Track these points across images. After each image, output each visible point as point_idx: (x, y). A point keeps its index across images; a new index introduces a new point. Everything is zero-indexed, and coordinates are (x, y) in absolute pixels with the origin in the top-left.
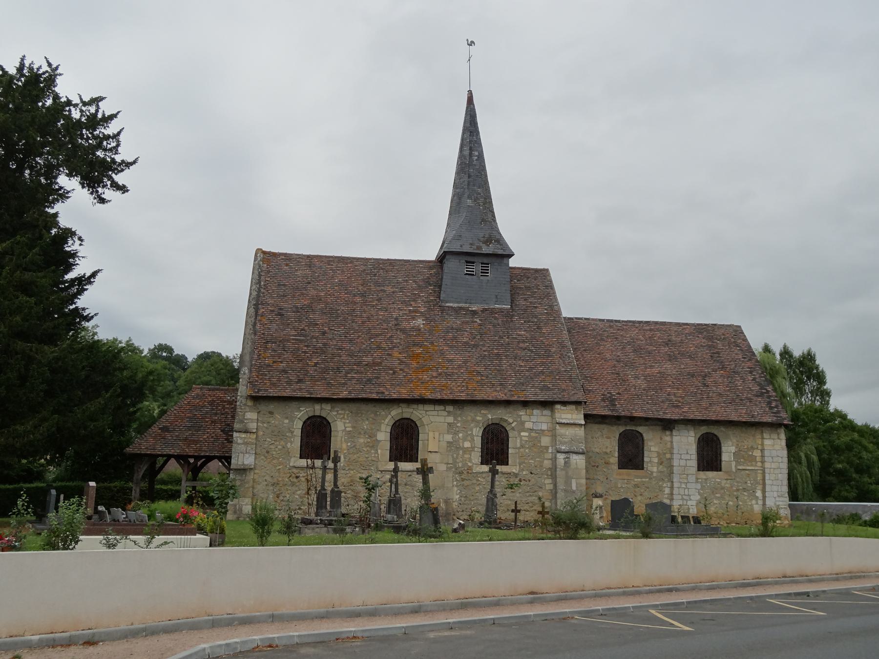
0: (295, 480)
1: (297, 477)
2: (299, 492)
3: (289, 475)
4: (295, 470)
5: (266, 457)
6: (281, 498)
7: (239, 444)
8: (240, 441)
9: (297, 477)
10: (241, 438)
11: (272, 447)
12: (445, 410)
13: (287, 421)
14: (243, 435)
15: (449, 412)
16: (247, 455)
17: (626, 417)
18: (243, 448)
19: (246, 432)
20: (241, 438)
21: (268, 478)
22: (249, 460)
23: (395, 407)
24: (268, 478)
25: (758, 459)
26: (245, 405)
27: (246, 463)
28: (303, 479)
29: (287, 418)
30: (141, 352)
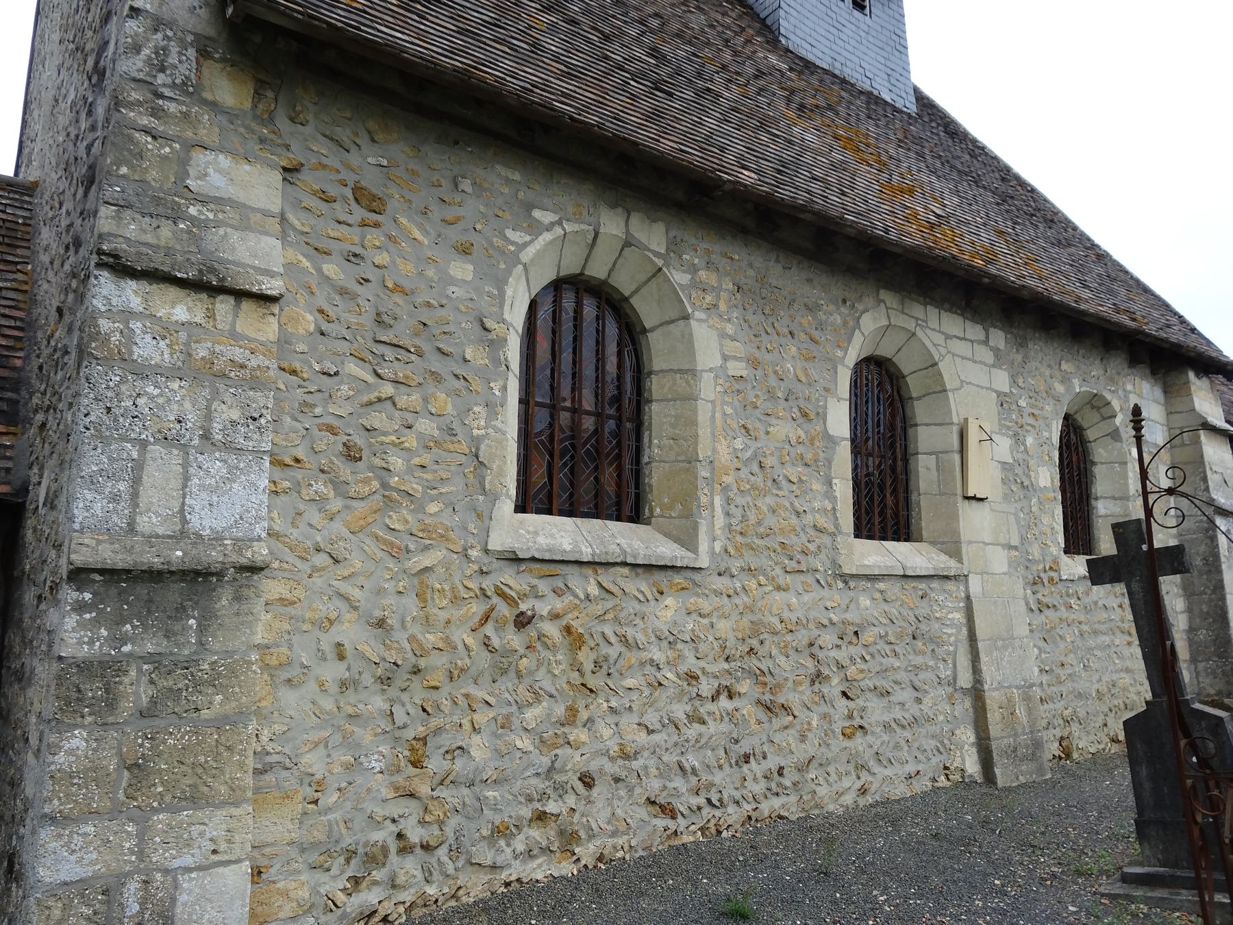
0: (515, 640)
1: (522, 621)
2: (532, 715)
3: (477, 609)
4: (510, 578)
5: (339, 486)
6: (435, 764)
7: (142, 372)
8: (147, 349)
9: (522, 621)
10: (166, 330)
11: (377, 419)
12: (986, 342)
13: (462, 270)
14: (181, 309)
15: (996, 351)
16: (216, 466)
17: (741, 195)
18: (179, 402)
19: (207, 285)
20: (166, 330)
21: (351, 632)
22: (226, 504)
23: (888, 297)
24: (351, 632)
25: (1203, 674)
26: (189, 90)
27: (204, 520)
28: (552, 630)
29: (465, 251)
30: (1197, 376)
